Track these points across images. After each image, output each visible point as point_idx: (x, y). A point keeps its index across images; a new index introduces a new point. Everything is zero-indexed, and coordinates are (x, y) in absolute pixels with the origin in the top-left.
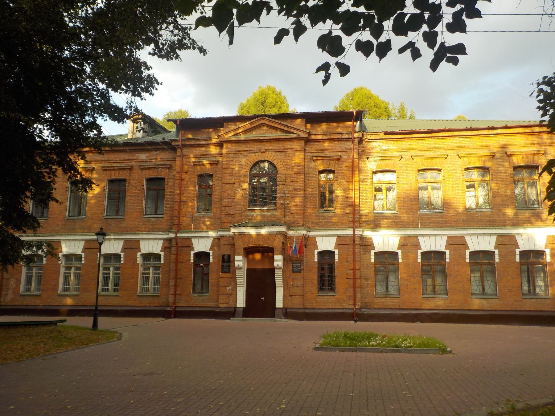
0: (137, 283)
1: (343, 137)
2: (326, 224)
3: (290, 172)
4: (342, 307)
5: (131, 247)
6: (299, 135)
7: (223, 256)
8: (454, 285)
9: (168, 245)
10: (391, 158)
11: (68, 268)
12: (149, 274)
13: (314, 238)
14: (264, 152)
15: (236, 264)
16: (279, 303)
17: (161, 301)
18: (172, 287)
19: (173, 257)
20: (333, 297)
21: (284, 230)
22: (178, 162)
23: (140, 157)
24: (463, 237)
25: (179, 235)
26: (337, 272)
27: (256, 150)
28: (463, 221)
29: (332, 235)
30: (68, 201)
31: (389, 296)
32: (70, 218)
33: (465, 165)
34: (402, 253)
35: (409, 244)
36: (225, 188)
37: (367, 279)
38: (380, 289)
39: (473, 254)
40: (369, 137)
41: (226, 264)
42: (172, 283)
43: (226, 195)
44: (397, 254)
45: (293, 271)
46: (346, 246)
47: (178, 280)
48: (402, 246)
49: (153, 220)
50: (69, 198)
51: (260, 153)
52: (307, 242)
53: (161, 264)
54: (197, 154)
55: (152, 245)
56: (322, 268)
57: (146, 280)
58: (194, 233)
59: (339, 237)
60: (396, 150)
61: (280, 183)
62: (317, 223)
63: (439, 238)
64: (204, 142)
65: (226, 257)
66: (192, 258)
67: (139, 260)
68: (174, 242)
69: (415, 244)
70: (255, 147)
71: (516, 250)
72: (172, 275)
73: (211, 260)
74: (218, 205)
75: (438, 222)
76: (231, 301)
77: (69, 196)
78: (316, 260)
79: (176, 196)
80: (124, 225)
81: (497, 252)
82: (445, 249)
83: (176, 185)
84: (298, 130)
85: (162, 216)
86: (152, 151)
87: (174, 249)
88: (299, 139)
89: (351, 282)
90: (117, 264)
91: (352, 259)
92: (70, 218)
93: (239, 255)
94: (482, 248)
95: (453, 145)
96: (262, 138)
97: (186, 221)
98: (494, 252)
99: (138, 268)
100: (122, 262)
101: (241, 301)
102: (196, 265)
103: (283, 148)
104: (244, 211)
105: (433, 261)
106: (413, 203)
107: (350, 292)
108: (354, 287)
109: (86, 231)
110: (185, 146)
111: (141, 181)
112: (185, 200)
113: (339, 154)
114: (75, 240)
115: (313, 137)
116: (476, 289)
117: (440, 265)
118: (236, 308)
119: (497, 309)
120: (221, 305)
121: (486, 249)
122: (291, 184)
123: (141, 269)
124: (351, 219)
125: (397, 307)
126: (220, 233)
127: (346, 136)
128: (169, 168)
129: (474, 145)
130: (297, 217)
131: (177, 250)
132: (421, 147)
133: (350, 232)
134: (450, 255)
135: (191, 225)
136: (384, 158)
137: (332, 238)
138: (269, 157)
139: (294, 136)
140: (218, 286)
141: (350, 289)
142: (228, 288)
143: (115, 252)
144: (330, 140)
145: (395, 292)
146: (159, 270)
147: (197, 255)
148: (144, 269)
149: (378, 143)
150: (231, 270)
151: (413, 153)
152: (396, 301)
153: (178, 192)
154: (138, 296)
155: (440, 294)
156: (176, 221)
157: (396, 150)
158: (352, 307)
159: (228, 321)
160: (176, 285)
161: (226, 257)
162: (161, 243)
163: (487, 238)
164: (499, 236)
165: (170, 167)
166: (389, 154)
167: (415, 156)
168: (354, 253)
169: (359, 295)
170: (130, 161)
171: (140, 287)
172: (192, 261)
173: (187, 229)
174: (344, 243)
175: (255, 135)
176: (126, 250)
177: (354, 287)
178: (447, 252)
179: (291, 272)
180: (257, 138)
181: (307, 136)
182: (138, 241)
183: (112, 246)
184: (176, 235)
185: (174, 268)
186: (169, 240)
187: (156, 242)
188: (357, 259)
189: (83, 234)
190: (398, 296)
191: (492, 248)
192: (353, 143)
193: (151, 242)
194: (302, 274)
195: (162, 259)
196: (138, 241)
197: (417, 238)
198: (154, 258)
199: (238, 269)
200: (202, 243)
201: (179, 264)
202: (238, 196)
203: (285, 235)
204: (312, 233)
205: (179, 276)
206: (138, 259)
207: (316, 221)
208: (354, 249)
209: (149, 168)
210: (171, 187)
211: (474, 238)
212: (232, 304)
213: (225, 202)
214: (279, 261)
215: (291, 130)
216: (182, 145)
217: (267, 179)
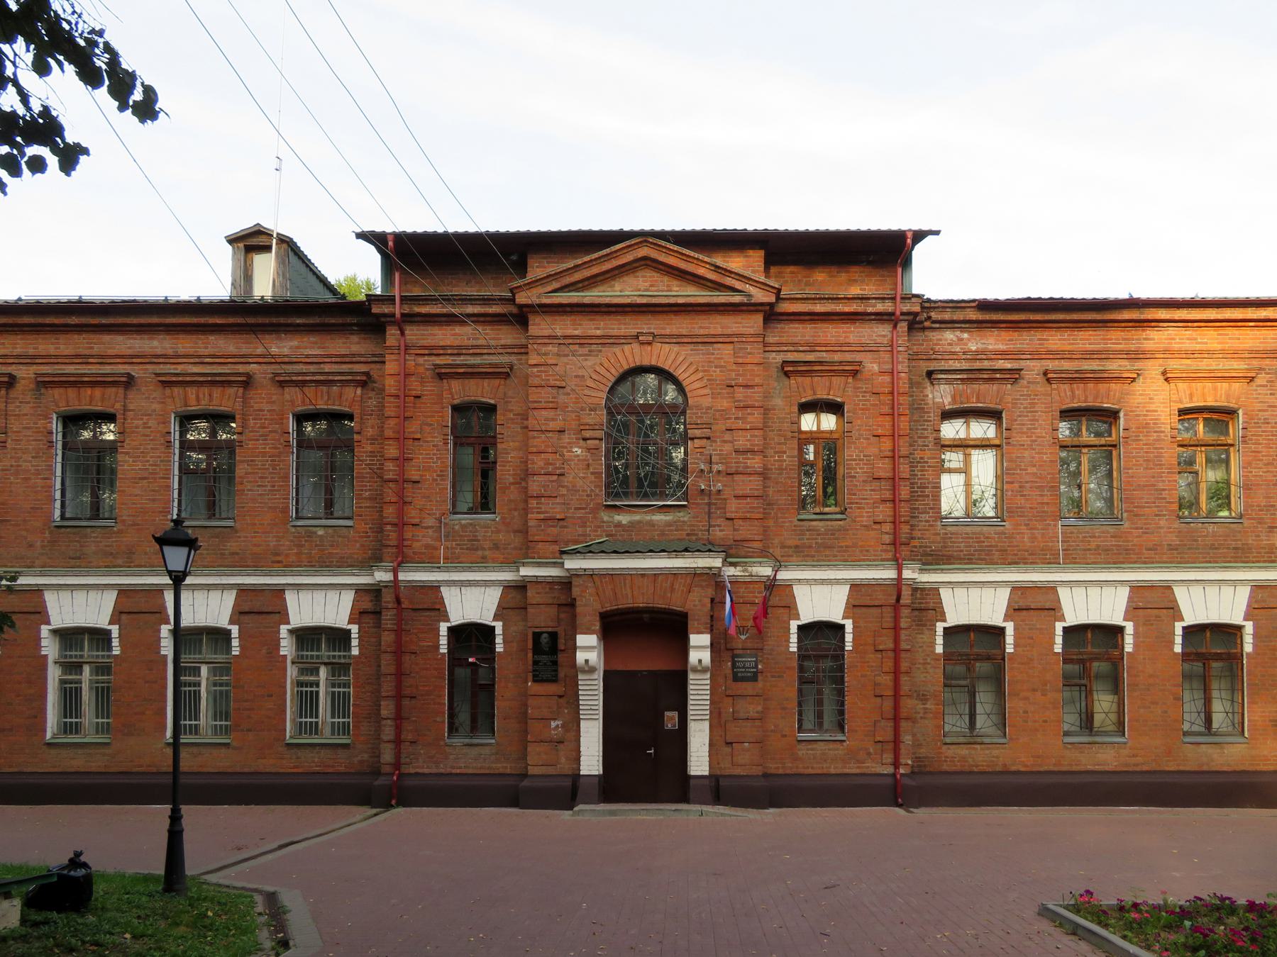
0: (285, 711)
1: (870, 310)
3: (725, 404)
5: (260, 609)
7: (537, 636)
8: (1142, 710)
9: (371, 605)
10: (993, 376)
11: (72, 667)
12: (318, 685)
13: (788, 586)
14: (649, 343)
15: (581, 657)
16: (699, 763)
17: (356, 760)
18: (389, 722)
19: (388, 638)
20: (838, 745)
21: (717, 562)
22: (391, 366)
24: (1170, 588)
25: (402, 576)
27: (625, 337)
28: (1171, 548)
29: (838, 582)
30: (59, 473)
31: (979, 740)
32: (66, 523)
33: (1181, 402)
34: (1255, 627)
35: (1033, 606)
36: (535, 442)
37: (923, 698)
38: (955, 723)
39: (1193, 632)
41: (544, 658)
42: (387, 709)
43: (541, 464)
44: (1000, 631)
45: (736, 678)
47: (406, 702)
49: (321, 532)
50: (59, 467)
51: (636, 346)
52: (776, 598)
53: (350, 657)
55: (322, 604)
57: (308, 702)
58: (447, 570)
59: (856, 587)
60: (1003, 354)
61: (697, 433)
62: (797, 547)
65: (545, 639)
66: (443, 641)
67: (287, 647)
68: (388, 597)
69: (1048, 605)
71: (442, 624)
72: (388, 687)
73: (499, 648)
74: (514, 493)
76: (563, 760)
77: (59, 459)
78: (793, 648)
79: (390, 466)
80: (232, 546)
83: (388, 433)
84: (747, 279)
85: (349, 523)
87: (388, 618)
88: (748, 308)
89: (888, 704)
90: (220, 657)
91: (891, 646)
92: (66, 523)
93: (588, 631)
96: (644, 301)
97: (420, 540)
99: (285, 670)
100: (236, 651)
101: (591, 761)
102: (455, 658)
103: (702, 332)
104: (595, 511)
107: (886, 731)
108: (896, 719)
109: (120, 562)
110: (409, 318)
111: (281, 420)
113: (857, 357)
114: (209, 587)
115: (785, 307)
116: (1192, 721)
117: (1109, 659)
118: (576, 776)
120: (532, 771)
122: (727, 436)
123: (291, 672)
124: (887, 539)
126: (526, 571)
127: (880, 307)
128: (363, 384)
129: (1203, 347)
130: (745, 531)
131: (399, 620)
134: (1136, 635)
135: (437, 549)
136: (972, 376)
138: (662, 358)
139: (737, 299)
140: (523, 718)
141: (883, 723)
142: (553, 724)
143: (211, 622)
145: (992, 731)
146: (346, 674)
147: (458, 633)
148: (302, 671)
149: (958, 333)
150: (562, 673)
151: (1051, 365)
153: (392, 451)
154: (288, 745)
155: (1106, 734)
156: (393, 535)
157: (1003, 353)
158: (890, 770)
159: (566, 815)
160: (399, 718)
161: (545, 639)
162: (348, 598)
165: (365, 382)
166: (986, 364)
167: (1054, 372)
168: (896, 628)
169: (907, 739)
170: (244, 359)
171: (293, 721)
172: (444, 650)
173: (429, 559)
174: (869, 603)
176: (246, 618)
177: (896, 719)
178: (1129, 627)
179: (730, 682)
180: (629, 301)
181: (773, 299)
182: (279, 592)
183: (208, 606)
184: (396, 576)
185: (392, 669)
186: (374, 591)
187: (333, 595)
188: (904, 646)
189: (110, 567)
190: (1003, 741)
191: (1237, 619)
192: (895, 327)
193: (319, 595)
194: (760, 684)
195: (355, 642)
196: (279, 592)
197: (1054, 589)
198: (328, 640)
199: (584, 672)
200: (472, 601)
201: (407, 659)
203: (713, 577)
204: (783, 575)
205: (407, 692)
206: (164, 643)
207: (790, 543)
208: (896, 618)
209: (304, 383)
210: (373, 440)
211: (1197, 590)
212: (564, 767)
213: (535, 485)
214: (700, 648)
215: (729, 281)
216: (403, 315)
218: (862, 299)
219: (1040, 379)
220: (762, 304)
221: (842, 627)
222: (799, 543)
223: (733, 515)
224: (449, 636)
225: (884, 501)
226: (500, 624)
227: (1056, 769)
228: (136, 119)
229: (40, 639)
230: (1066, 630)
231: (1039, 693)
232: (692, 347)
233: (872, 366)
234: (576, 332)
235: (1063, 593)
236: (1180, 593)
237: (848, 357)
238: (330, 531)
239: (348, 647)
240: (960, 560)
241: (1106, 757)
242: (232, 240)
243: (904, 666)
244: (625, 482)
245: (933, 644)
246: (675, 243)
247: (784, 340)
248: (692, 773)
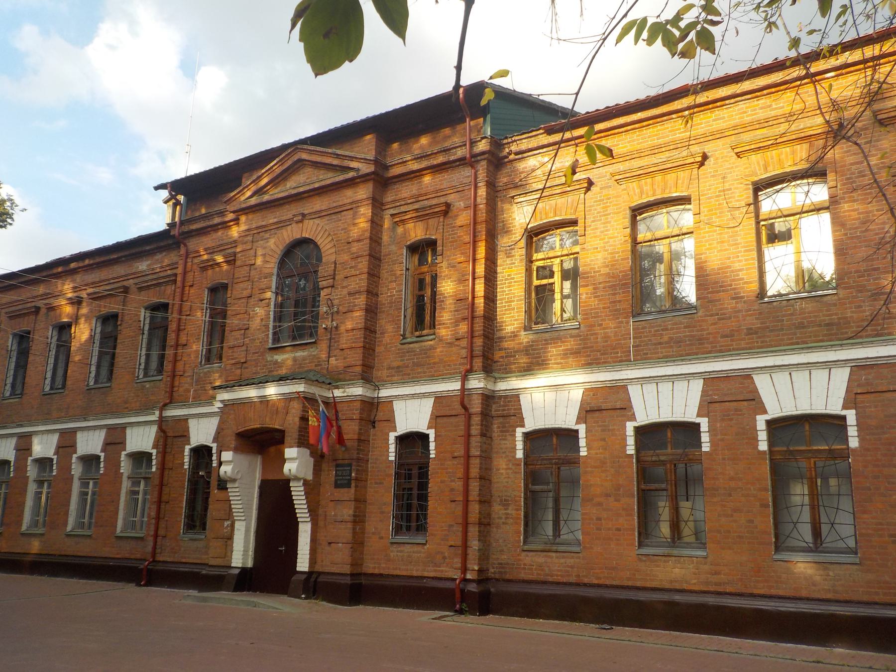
1: (452, 158)
2: (414, 370)
4: (439, 575)
5: (67, 444)
6: (358, 170)
13: (389, 403)
16: (303, 564)
20: (420, 548)
23: (140, 268)
24: (749, 377)
25: (456, 386)
26: (433, 487)
28: (750, 332)
39: (645, 433)
40: (514, 148)
44: (573, 434)
45: (337, 486)
46: (453, 420)
48: (587, 412)
52: (374, 413)
54: (209, 246)
62: (398, 367)
63: (681, 385)
64: (217, 220)
70: (287, 212)
71: (758, 417)
75: (679, 342)
81: (851, 416)
82: (698, 415)
86: (155, 254)
89: (459, 509)
94: (804, 408)
95: (721, 125)
101: (241, 553)
104: (263, 354)
105: (669, 451)
106: (618, 298)
112: (185, 342)
119: (855, 598)
121: (678, 416)
125: (573, 579)
132: (639, 147)
133: (454, 386)
137: (424, 401)
139: (351, 174)
144: (437, 169)
152: (570, 562)
163: (820, 375)
164: (859, 368)
175: (292, 185)
176: (109, 447)
202: (256, 323)
204: (384, 393)
207: (395, 364)
211: (782, 378)
217: (692, 298)
218: (444, 151)
219: (612, 182)
220: (367, 175)
221: (698, 425)
222: (400, 363)
223: (344, 346)
224: (525, 442)
225: (464, 319)
226: (433, 430)
227: (630, 583)
228: (308, 67)
229: (120, 462)
230: (639, 430)
231: (612, 499)
232: (327, 218)
233: (458, 203)
234: (264, 223)
235: (634, 391)
236: (762, 383)
238: (152, 384)
239: (149, 465)
241: (677, 571)
244: (845, 254)
245: (514, 449)
246: (312, 145)
247: (398, 197)
248: (298, 569)
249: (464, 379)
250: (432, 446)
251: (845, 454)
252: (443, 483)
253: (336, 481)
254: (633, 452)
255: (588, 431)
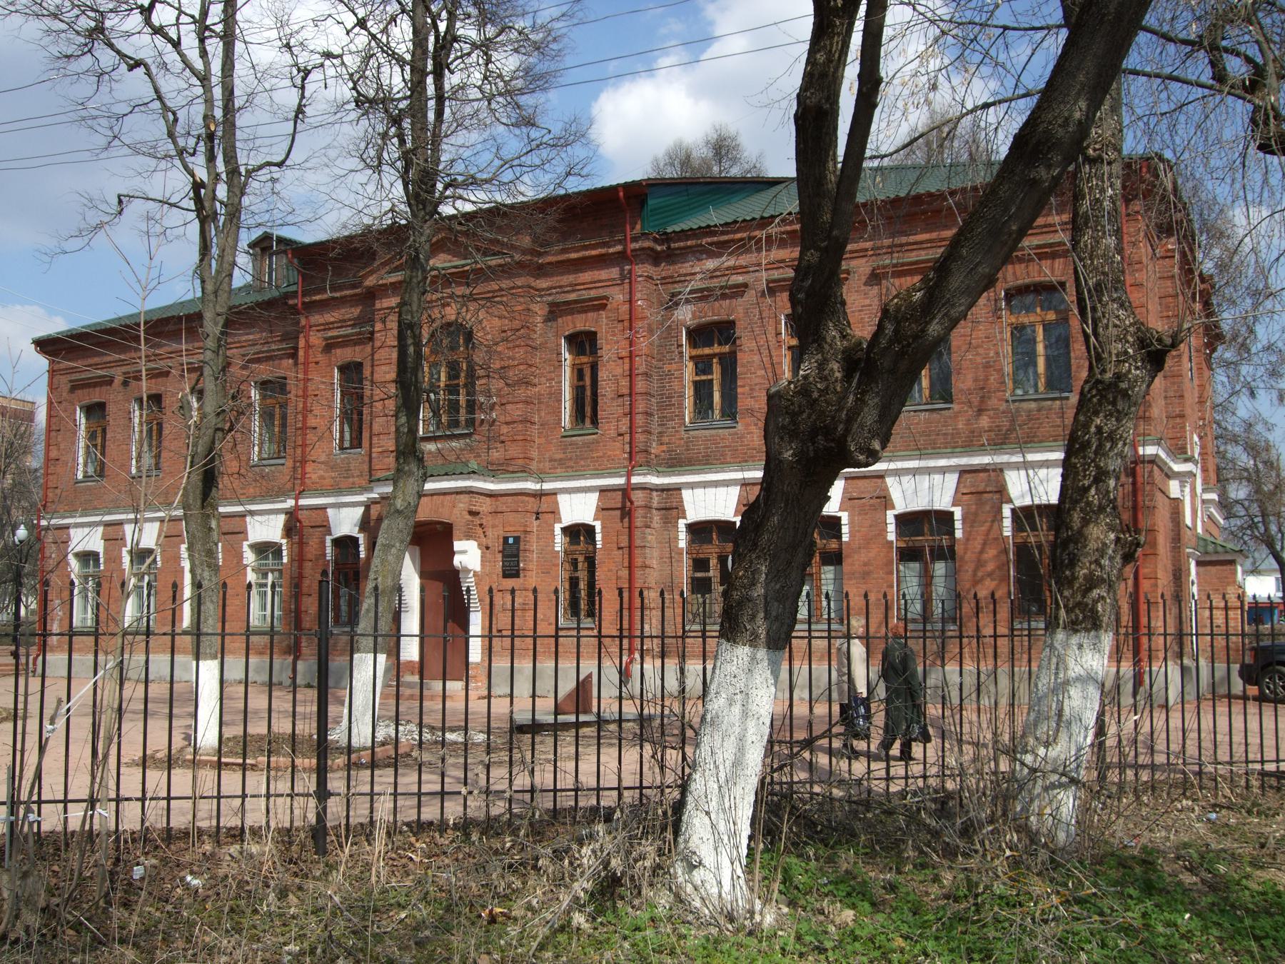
9: (621, 506)
25: (635, 480)
32: (264, 462)
39: (904, 521)
56: (574, 563)
92: (264, 462)
98: (952, 514)
113: (601, 292)
134: (851, 523)
164: (964, 472)
182: (999, 470)
188: (638, 542)
207: (557, 456)
221: (357, 539)
222: (562, 456)
237: (593, 294)
240: (699, 462)
242: (45, 345)
243: (638, 561)
249: (629, 476)
250: (599, 537)
251: (217, 565)
252: (609, 576)
253: (504, 571)
254: (1009, 534)
255: (603, 527)
